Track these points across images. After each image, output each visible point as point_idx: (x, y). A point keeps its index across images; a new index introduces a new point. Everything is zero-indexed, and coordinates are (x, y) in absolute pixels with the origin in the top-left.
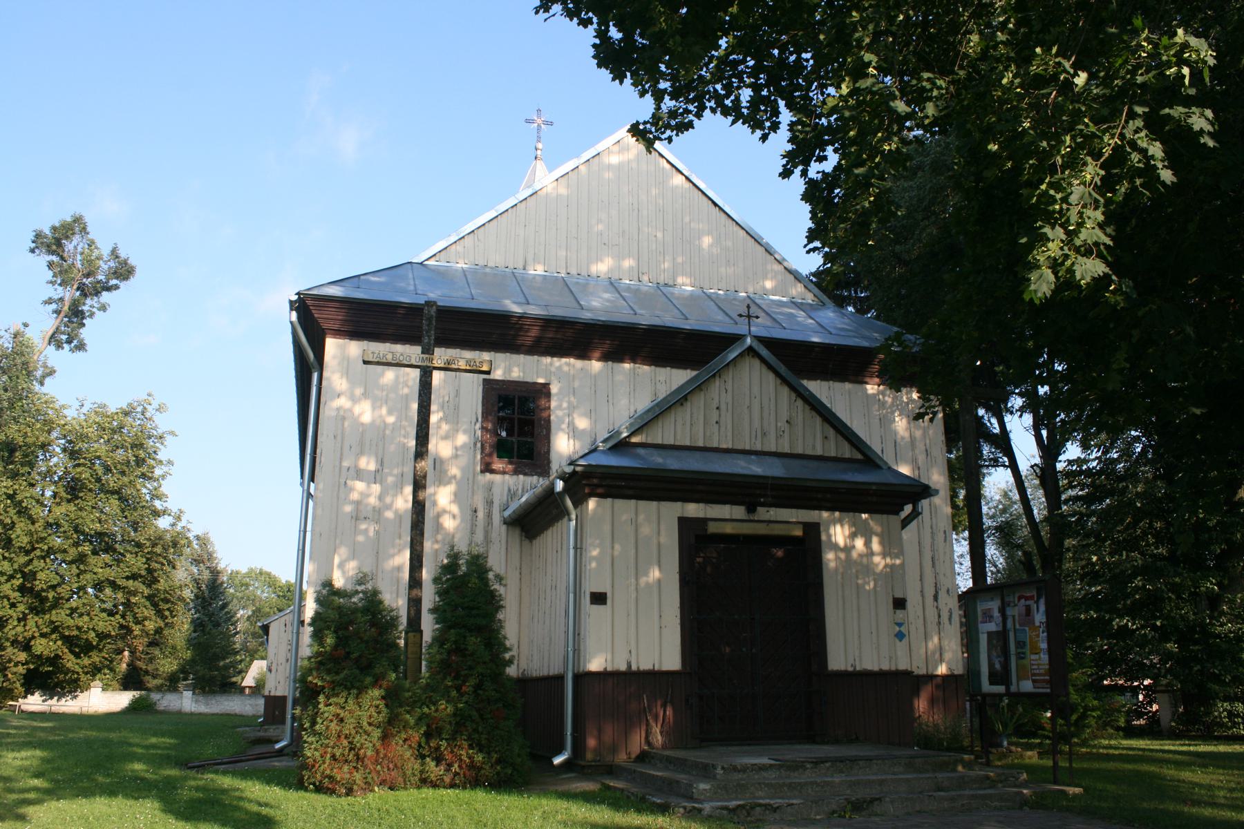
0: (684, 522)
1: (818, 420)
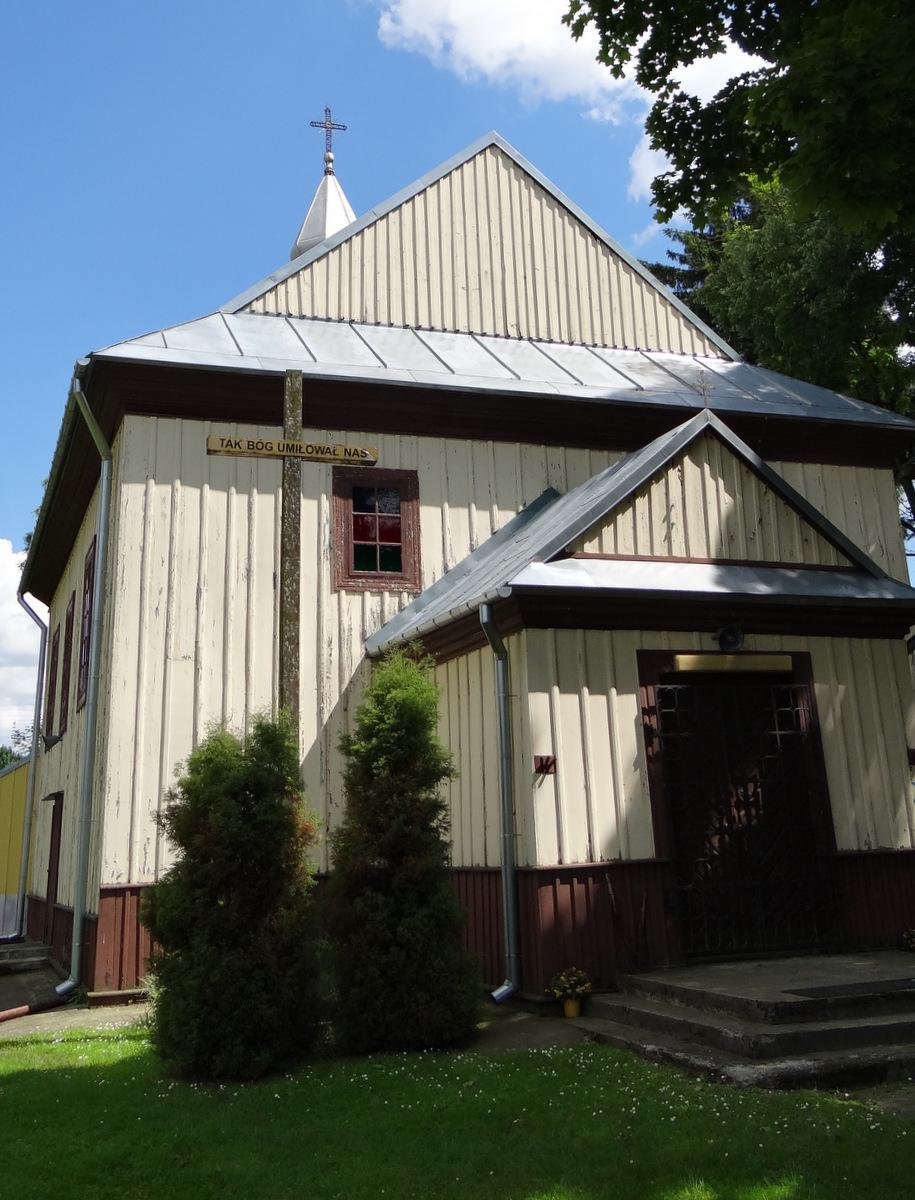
0: (334, 467)
1: (795, 517)
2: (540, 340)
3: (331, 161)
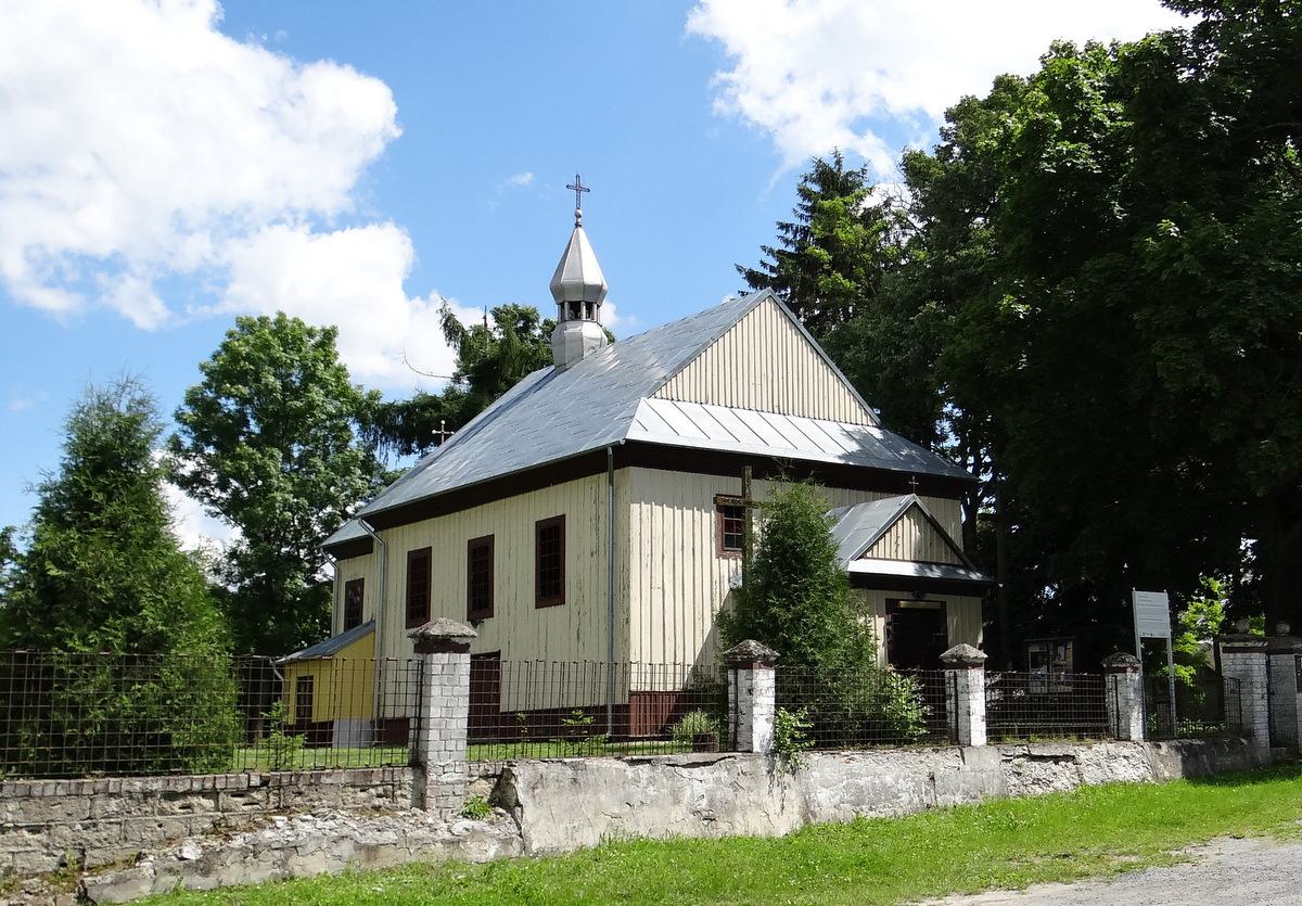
3: (580, 216)
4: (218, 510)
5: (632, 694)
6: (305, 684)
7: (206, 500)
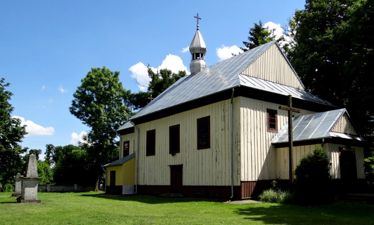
2: (267, 80)
4: (85, 122)
5: (241, 182)
6: (113, 174)
7: (82, 119)
